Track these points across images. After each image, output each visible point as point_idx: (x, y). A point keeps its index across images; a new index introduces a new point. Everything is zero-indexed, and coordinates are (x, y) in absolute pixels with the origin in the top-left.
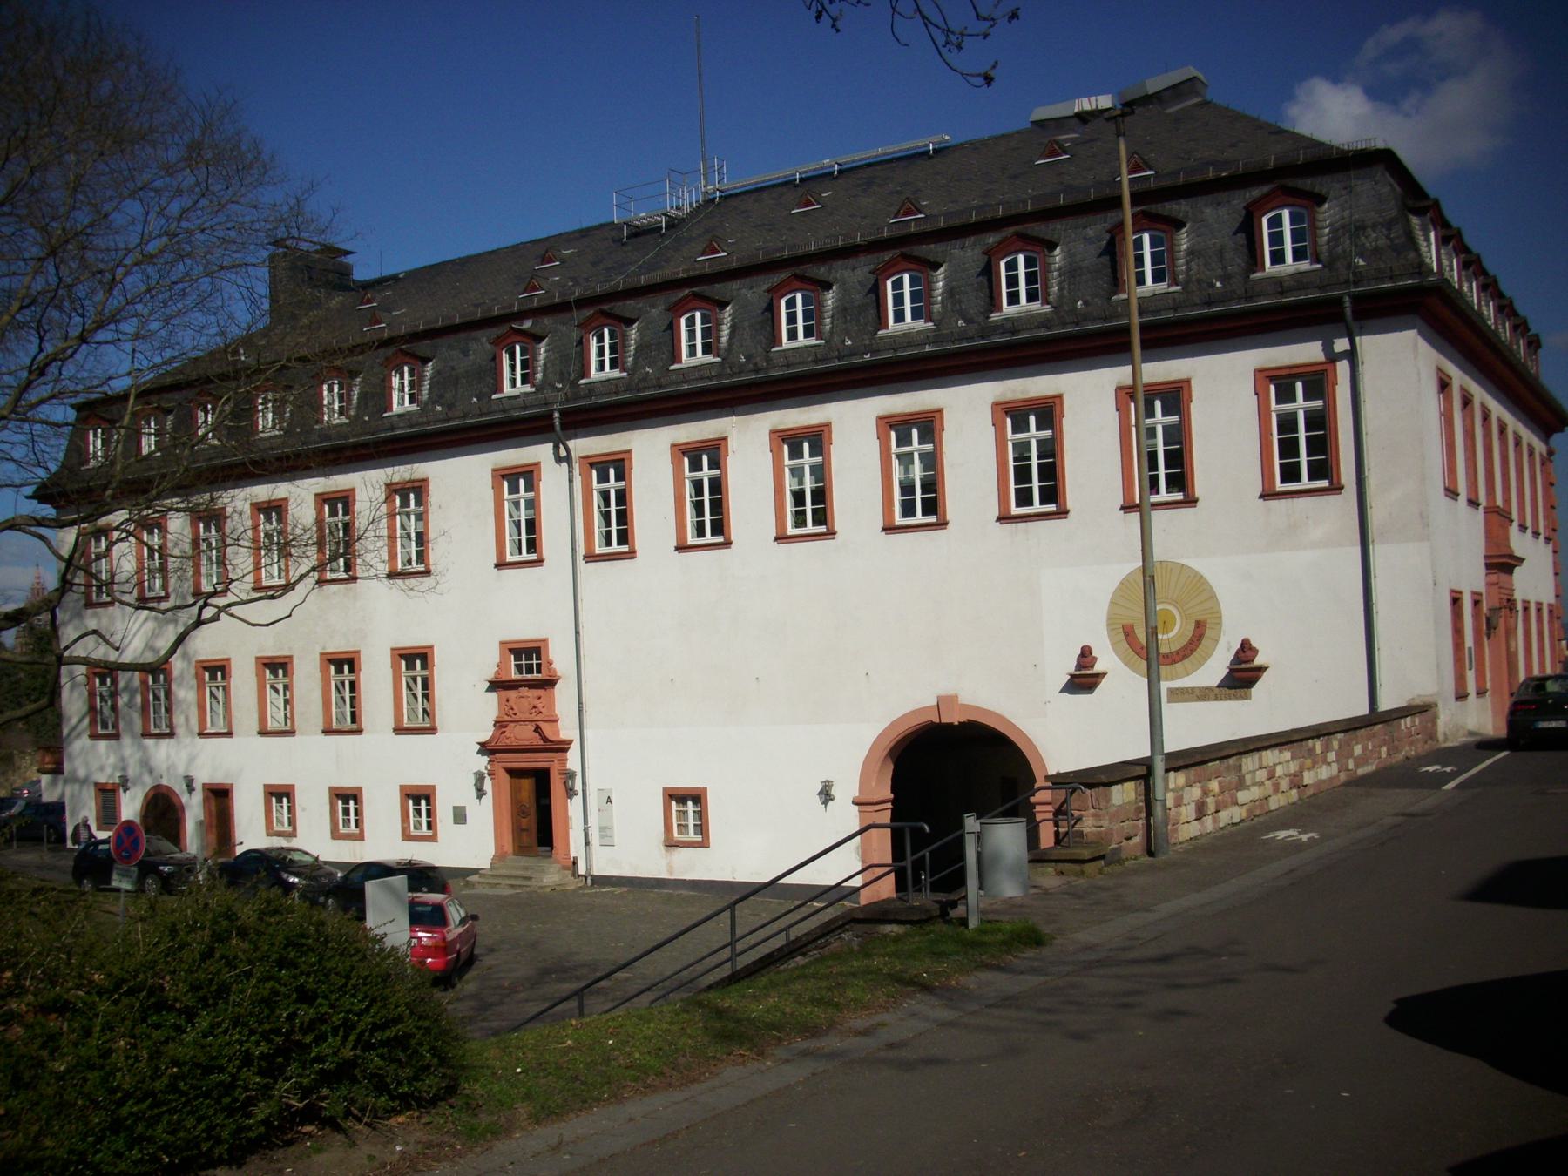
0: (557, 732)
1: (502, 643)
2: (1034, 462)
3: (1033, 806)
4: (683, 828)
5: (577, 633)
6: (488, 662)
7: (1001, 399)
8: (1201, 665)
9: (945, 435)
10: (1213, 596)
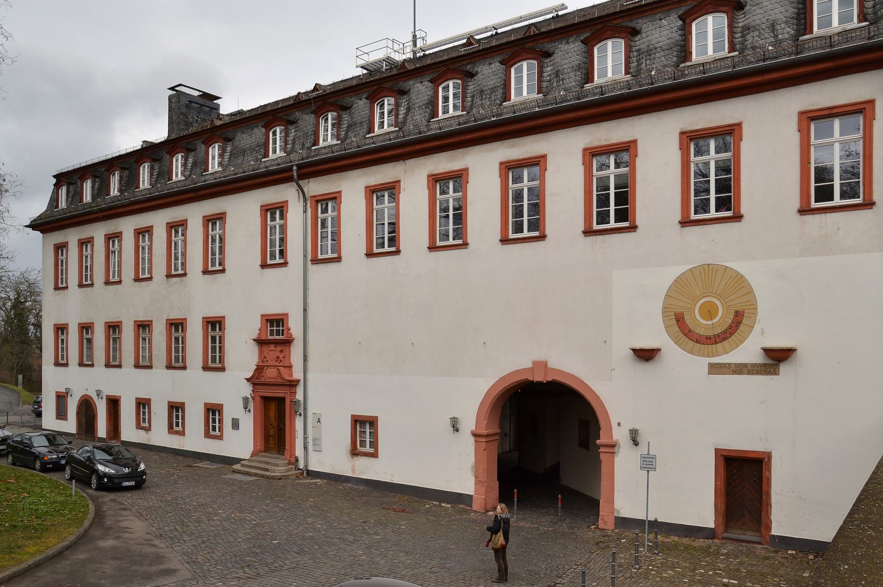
0: (291, 375)
1: (262, 316)
2: (612, 192)
3: (599, 447)
4: (363, 444)
5: (305, 310)
6: (254, 327)
7: (589, 146)
8: (737, 346)
9: (288, 214)
10: (751, 292)
